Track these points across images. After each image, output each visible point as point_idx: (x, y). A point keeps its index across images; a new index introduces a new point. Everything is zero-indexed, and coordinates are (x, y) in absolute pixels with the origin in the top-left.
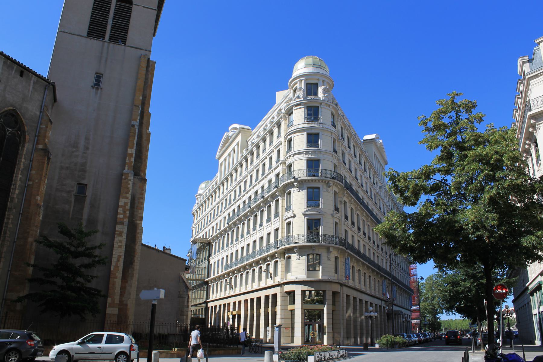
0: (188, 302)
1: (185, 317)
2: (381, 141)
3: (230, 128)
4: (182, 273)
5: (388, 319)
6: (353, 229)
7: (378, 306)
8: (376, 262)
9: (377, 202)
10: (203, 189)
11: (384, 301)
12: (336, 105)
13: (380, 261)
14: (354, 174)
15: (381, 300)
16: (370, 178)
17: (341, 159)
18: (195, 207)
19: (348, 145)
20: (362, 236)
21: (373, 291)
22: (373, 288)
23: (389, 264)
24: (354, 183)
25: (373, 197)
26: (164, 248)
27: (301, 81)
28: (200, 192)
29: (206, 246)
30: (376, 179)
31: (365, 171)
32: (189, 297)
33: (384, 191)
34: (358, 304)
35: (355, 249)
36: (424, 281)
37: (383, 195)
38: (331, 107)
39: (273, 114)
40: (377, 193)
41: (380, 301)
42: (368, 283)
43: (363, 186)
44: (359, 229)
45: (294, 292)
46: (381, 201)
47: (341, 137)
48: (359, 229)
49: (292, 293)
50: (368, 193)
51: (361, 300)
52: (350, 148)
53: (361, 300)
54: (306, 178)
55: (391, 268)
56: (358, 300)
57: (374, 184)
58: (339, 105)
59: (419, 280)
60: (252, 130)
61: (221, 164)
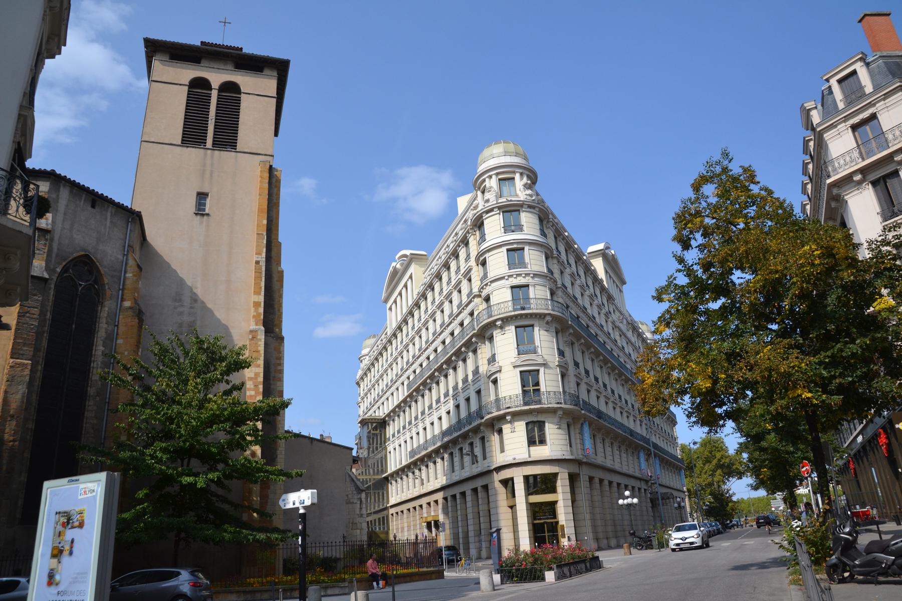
27: (490, 177)
29: (376, 429)
45: (512, 479)
49: (510, 482)
54: (513, 313)
61: (390, 309)
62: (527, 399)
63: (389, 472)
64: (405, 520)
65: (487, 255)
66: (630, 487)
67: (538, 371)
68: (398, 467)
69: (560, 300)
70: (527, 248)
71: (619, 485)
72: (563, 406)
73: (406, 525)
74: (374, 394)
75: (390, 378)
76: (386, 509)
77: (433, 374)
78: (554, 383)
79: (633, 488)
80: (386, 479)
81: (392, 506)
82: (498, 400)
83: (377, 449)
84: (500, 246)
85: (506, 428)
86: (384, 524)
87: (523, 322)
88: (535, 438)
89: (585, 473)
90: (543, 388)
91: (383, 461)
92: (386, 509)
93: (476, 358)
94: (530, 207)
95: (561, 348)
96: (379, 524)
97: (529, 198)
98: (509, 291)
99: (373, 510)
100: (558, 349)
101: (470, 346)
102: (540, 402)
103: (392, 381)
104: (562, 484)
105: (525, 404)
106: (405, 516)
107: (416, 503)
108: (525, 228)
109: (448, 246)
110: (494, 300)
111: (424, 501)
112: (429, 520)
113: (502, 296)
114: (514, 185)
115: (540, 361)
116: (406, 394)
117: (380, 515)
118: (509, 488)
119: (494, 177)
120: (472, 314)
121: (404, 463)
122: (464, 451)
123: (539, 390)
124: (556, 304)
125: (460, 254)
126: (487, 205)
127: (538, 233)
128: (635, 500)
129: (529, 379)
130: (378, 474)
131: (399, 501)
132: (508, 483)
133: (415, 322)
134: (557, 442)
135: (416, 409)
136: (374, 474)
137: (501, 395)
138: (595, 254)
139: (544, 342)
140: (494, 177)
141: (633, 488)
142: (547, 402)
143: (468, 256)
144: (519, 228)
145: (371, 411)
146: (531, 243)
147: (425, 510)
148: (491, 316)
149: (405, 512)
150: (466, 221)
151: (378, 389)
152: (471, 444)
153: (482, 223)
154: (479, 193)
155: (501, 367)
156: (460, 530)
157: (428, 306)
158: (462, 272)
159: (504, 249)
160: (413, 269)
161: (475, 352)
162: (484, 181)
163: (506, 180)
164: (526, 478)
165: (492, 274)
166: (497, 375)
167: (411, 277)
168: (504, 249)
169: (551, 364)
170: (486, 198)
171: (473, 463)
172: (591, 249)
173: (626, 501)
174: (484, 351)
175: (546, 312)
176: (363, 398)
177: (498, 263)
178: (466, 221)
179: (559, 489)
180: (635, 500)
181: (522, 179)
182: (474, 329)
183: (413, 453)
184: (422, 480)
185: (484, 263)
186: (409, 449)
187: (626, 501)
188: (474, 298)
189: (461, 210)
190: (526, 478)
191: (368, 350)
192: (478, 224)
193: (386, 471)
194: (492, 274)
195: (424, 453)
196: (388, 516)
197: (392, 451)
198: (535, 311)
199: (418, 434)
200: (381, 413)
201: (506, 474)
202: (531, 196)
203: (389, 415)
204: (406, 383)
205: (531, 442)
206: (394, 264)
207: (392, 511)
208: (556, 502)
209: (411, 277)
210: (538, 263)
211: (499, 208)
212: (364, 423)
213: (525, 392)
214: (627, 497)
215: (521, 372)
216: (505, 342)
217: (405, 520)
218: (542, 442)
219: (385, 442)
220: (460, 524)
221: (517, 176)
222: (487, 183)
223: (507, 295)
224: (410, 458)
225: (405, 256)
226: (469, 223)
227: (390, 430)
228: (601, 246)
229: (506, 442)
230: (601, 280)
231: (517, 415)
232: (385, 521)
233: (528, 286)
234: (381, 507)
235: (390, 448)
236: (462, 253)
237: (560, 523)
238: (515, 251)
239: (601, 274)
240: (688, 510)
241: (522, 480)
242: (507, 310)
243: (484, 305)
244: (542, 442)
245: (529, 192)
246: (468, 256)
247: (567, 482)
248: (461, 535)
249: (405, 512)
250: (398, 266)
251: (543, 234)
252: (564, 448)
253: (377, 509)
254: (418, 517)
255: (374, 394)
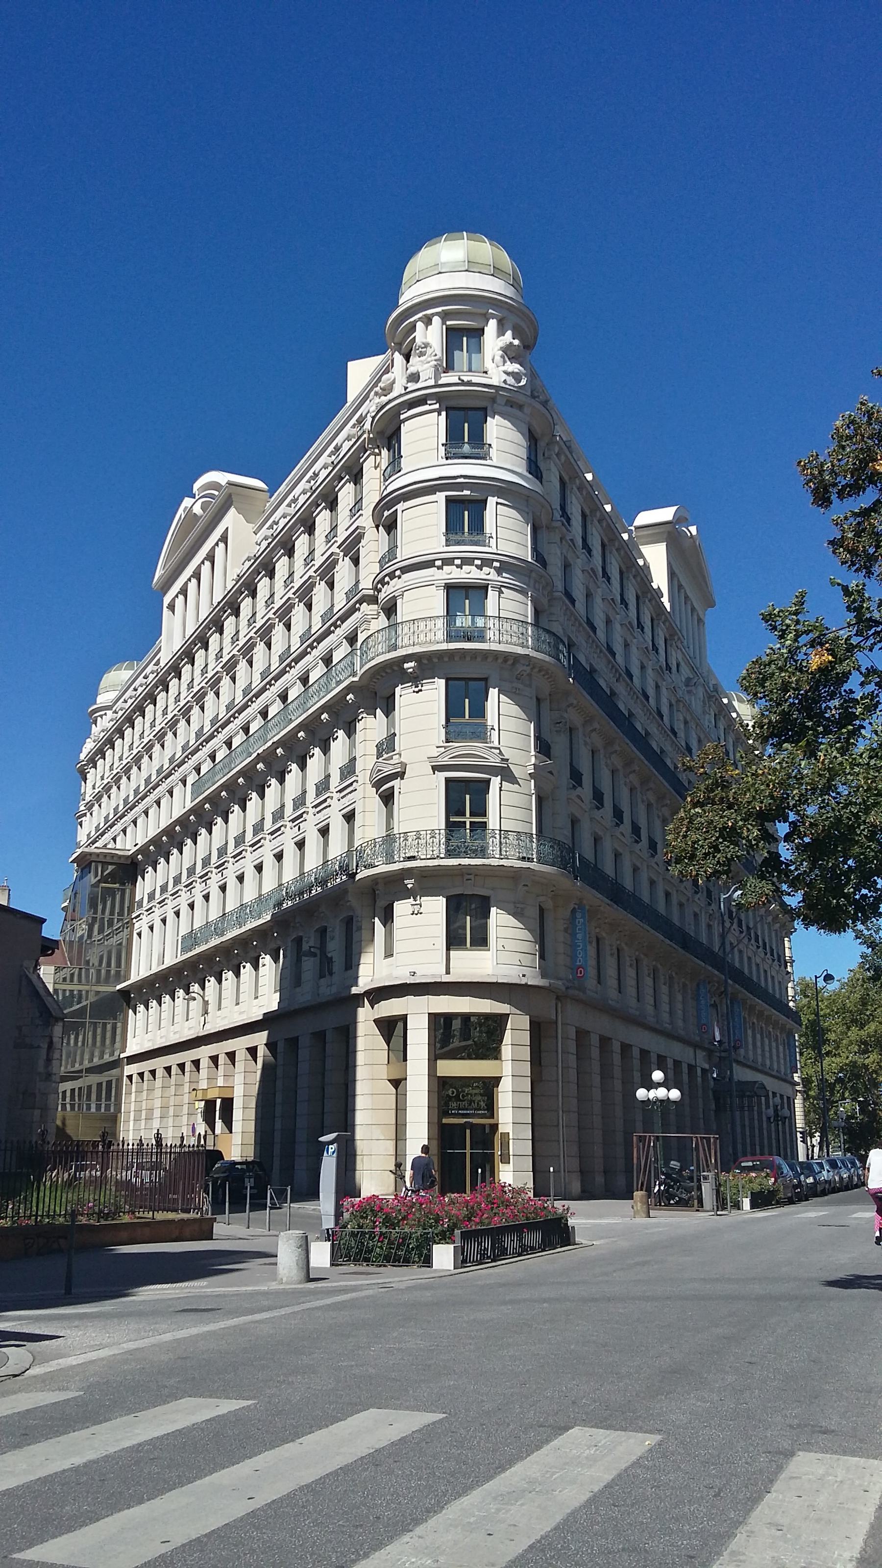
0: (49, 1060)
1: (37, 1112)
2: (693, 530)
3: (196, 486)
4: (28, 964)
5: (718, 1110)
6: (637, 847)
7: (685, 1069)
8: (676, 920)
9: (679, 726)
10: (115, 685)
11: (703, 1049)
12: (545, 404)
13: (689, 918)
14: (580, 605)
15: (696, 1046)
16: (655, 648)
17: (559, 585)
18: (89, 746)
19: (584, 540)
20: (628, 838)
21: (665, 1017)
22: (665, 1007)
23: (717, 929)
24: (600, 665)
25: (665, 711)
26: (275, 992)
27: (428, 321)
28: (103, 699)
29: (115, 877)
30: (675, 657)
31: (640, 626)
32: (51, 1043)
33: (700, 691)
34: (617, 1058)
35: (604, 877)
36: (833, 986)
37: (696, 705)
38: (527, 410)
39: (342, 436)
40: (678, 701)
41: (690, 1051)
42: (648, 991)
43: (630, 676)
44: (618, 814)
45: (404, 1018)
46: (692, 725)
47: (557, 515)
48: (598, 796)
49: (400, 1025)
50: (647, 698)
51: (605, 1041)
52: (589, 551)
53: (626, 1048)
54: (444, 646)
55: (723, 944)
56: (616, 1047)
57: (669, 668)
58: (551, 403)
59: (821, 983)
60: (272, 492)
61: (172, 607)
62: (454, 843)
63: (134, 978)
64: (158, 1093)
65: (400, 507)
66: (670, 1063)
67: (488, 782)
68: (155, 969)
69: (557, 628)
70: (492, 501)
71: (644, 1053)
72: (534, 866)
73: (158, 1103)
74: (116, 799)
75: (156, 764)
76: (116, 1064)
77: (253, 765)
78: (520, 814)
79: (677, 1063)
80: (125, 994)
81: (132, 1059)
82: (389, 839)
83: (111, 923)
84: (431, 490)
85: (402, 908)
86: (108, 1098)
87: (466, 680)
88: (465, 926)
89: (573, 1017)
90: (493, 822)
91: (122, 955)
92: (116, 1064)
93: (353, 745)
94: (510, 403)
95: (545, 736)
96: (99, 1098)
97: (511, 380)
98: (441, 595)
99: (86, 1064)
100: (538, 738)
101: (342, 716)
102: (482, 852)
103: (159, 772)
104: (515, 1042)
105: (450, 854)
106: (159, 1082)
107: (186, 1056)
108: (493, 452)
109: (337, 448)
110: (404, 612)
111: (204, 1053)
112: (210, 1096)
113: (423, 606)
114: (479, 349)
115: (494, 760)
116: (189, 805)
117: (103, 1078)
118: (396, 1040)
119: (436, 320)
120: (352, 639)
121: (169, 961)
122: (305, 947)
123: (484, 825)
124: (544, 636)
125: (340, 495)
126: (412, 386)
127: (522, 469)
128: (675, 1094)
129: (465, 797)
130: (107, 981)
131: (148, 1046)
132: (392, 1029)
133: (222, 645)
134: (511, 945)
135: (207, 843)
136: (98, 981)
137: (399, 828)
138: (656, 532)
139: (508, 727)
140: (436, 320)
141: (677, 1063)
142: (501, 855)
143: (359, 502)
144: (479, 447)
145: (108, 836)
146: (506, 491)
147: (204, 1072)
148: (394, 647)
149: (160, 1073)
150: (361, 420)
151: (127, 788)
152: (323, 931)
153: (396, 435)
154: (398, 358)
155: (404, 765)
156: (278, 1125)
157: (273, 590)
158: (340, 540)
159: (441, 497)
160: (232, 519)
161: (350, 732)
162: (413, 328)
163: (462, 337)
164: (434, 1018)
165: (407, 551)
166: (396, 783)
167: (224, 539)
168: (441, 497)
169: (517, 771)
170: (412, 370)
171: (322, 976)
172: (645, 518)
173: (653, 1094)
174: (371, 727)
175: (520, 651)
176: (90, 806)
177: (424, 526)
178: (361, 420)
179: (506, 1051)
180: (675, 1094)
181: (501, 332)
182: (354, 674)
183: (191, 940)
184: (206, 1003)
185: (391, 526)
186: (184, 930)
187: (653, 1094)
188: (360, 602)
189: (354, 390)
190: (434, 1018)
191: (112, 695)
192: (388, 435)
193: (127, 978)
194: (407, 551)
195: (214, 942)
196: (119, 1081)
197: (145, 931)
198: (494, 647)
199: (207, 897)
200: (129, 843)
201: (390, 1007)
202: (517, 376)
203: (144, 850)
204: (190, 780)
205: (454, 940)
206: (187, 502)
207: (129, 1070)
208: (498, 1080)
209: (224, 539)
210: (516, 537)
211: (439, 398)
212: (85, 863)
213: (452, 827)
214: (658, 1085)
215: (448, 781)
216: (422, 708)
217: (158, 1093)
218: (481, 941)
219: (131, 910)
220: (278, 1111)
221: (492, 326)
222: (420, 334)
223: (435, 602)
224: (185, 950)
225: (215, 486)
226: (367, 426)
227: (144, 887)
228: (666, 514)
229: (397, 934)
230: (659, 593)
231: (428, 881)
232: (110, 1093)
233: (485, 588)
234: (107, 1058)
235: (141, 925)
236: (346, 494)
237: (502, 1129)
238: (465, 512)
239: (660, 579)
240: (800, 1123)
241: (425, 1022)
242: (431, 636)
243: (382, 621)
244: (481, 941)
245: (515, 367)
246: (359, 502)
247: (526, 1038)
248: (278, 1138)
249: (160, 1073)
250: (197, 510)
251: (534, 468)
252: (527, 960)
253: (96, 1061)
254: (186, 1088)
255: (116, 799)
